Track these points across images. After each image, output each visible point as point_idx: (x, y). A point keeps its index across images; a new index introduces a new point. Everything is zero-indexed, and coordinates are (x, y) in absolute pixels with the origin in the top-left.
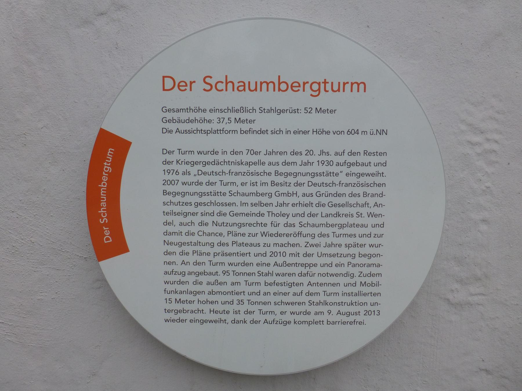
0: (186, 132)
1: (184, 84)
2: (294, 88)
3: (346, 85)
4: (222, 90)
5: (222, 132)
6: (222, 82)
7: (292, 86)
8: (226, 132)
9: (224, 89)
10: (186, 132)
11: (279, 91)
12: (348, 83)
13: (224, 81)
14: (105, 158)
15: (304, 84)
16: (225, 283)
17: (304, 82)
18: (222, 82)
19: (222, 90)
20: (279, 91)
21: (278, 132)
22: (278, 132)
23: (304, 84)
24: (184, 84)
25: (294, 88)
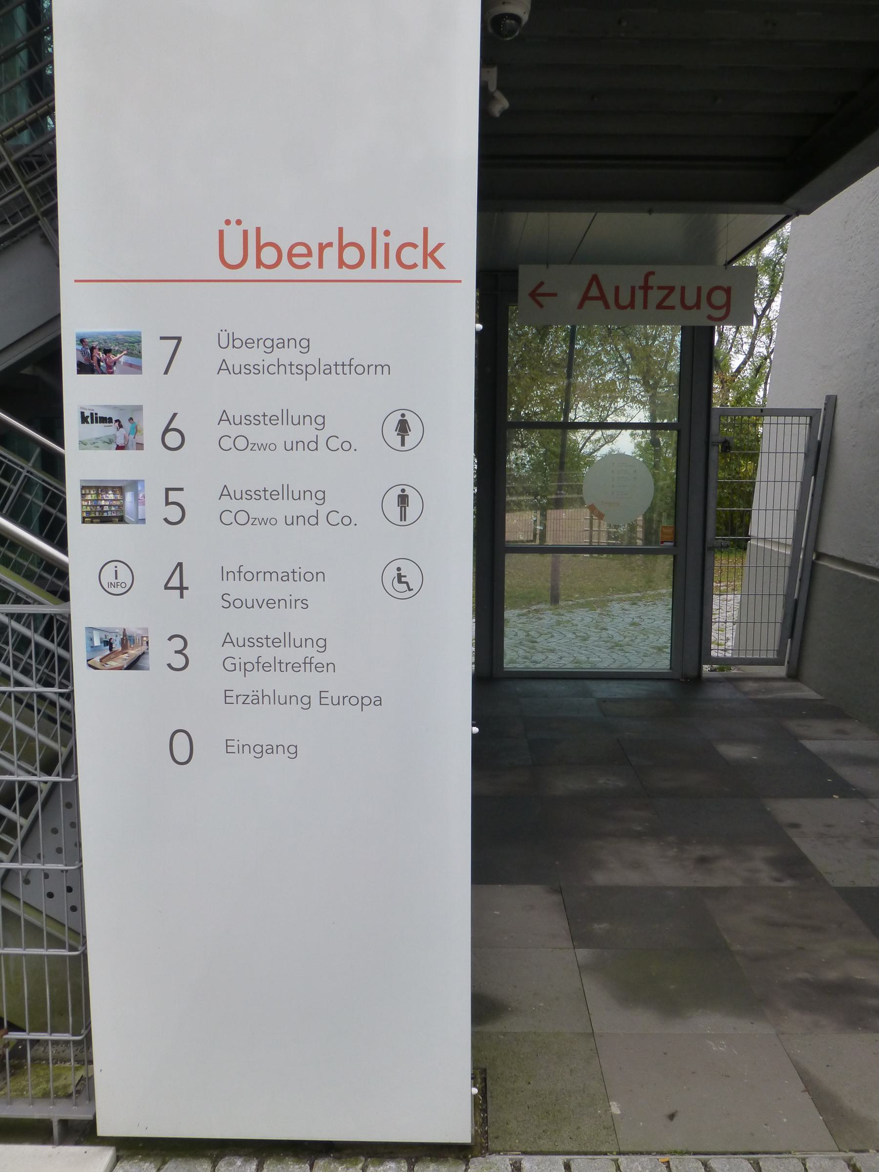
0: (248, 369)
1: (303, 250)
2: (296, 260)
3: (327, 251)
4: (415, 266)
5: (347, 368)
6: (415, 246)
7: (290, 255)
8: (360, 369)
9: (420, 263)
10: (248, 369)
11: (258, 267)
12: (330, 245)
13: (420, 244)
14: (662, 424)
15: (322, 248)
16: (331, 667)
17: (320, 244)
18: (415, 246)
19: (415, 266)
20: (258, 267)
21: (273, 369)
22: (273, 369)
23: (322, 248)
24: (303, 250)
25: (296, 260)
